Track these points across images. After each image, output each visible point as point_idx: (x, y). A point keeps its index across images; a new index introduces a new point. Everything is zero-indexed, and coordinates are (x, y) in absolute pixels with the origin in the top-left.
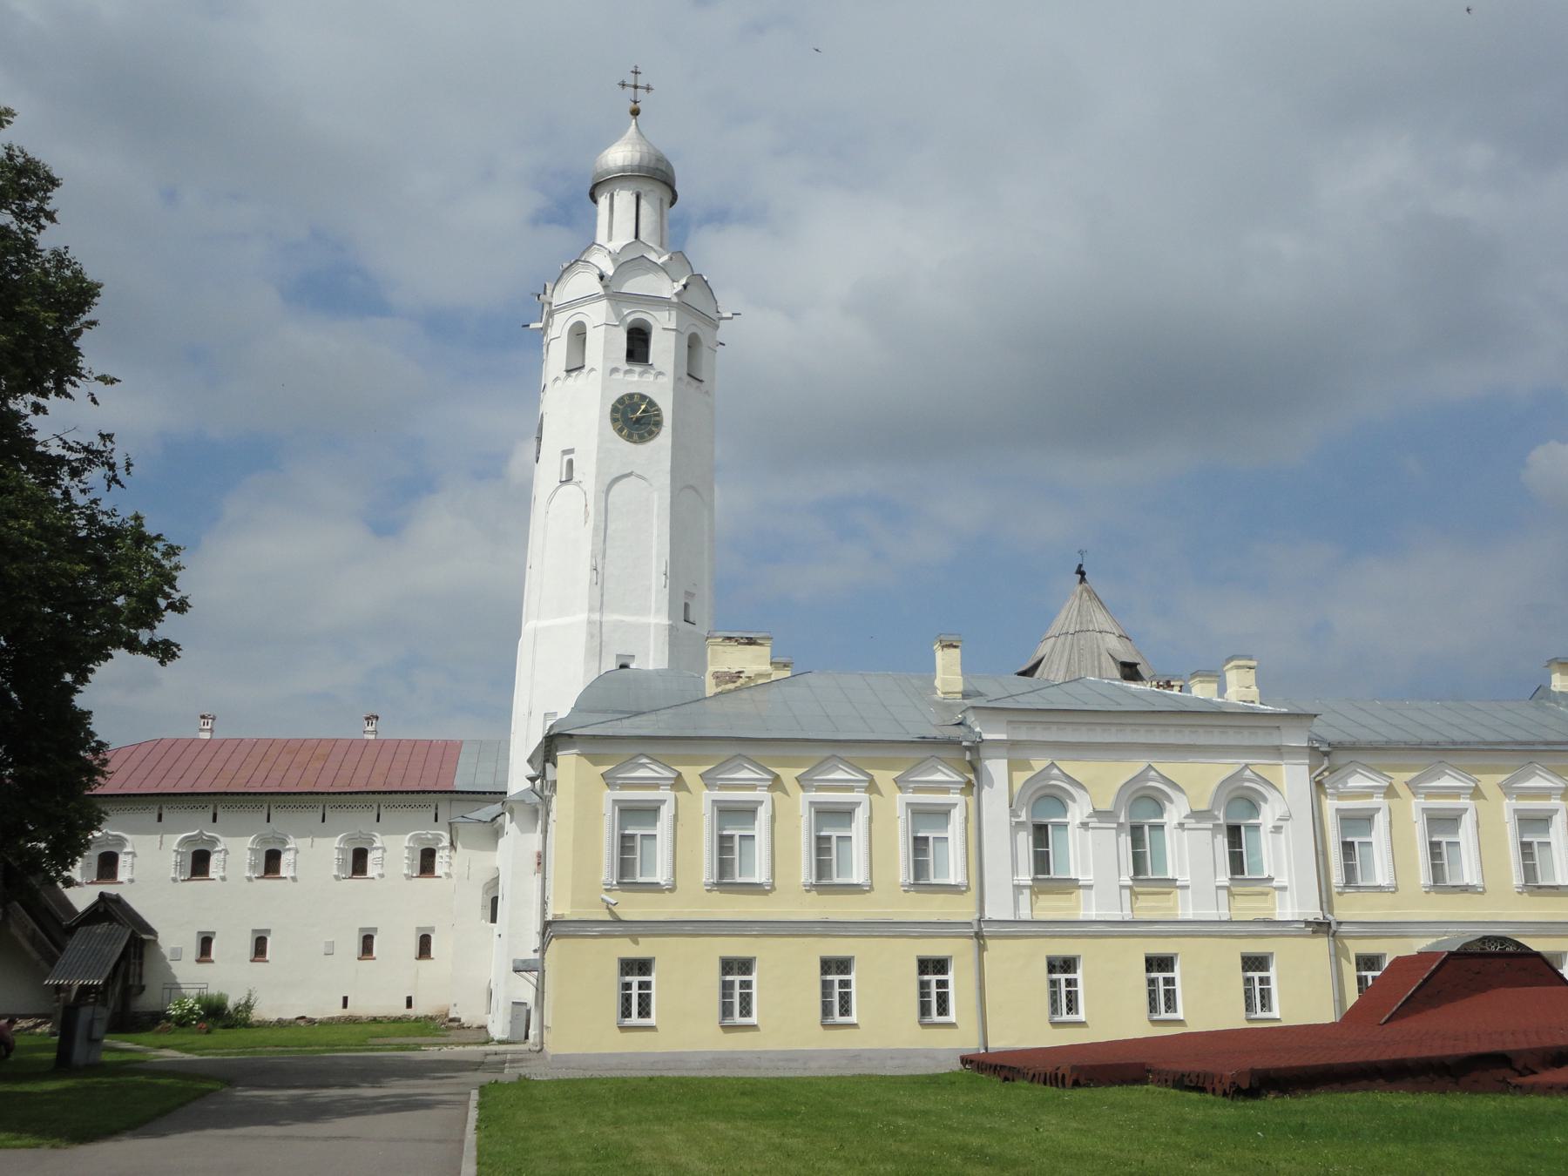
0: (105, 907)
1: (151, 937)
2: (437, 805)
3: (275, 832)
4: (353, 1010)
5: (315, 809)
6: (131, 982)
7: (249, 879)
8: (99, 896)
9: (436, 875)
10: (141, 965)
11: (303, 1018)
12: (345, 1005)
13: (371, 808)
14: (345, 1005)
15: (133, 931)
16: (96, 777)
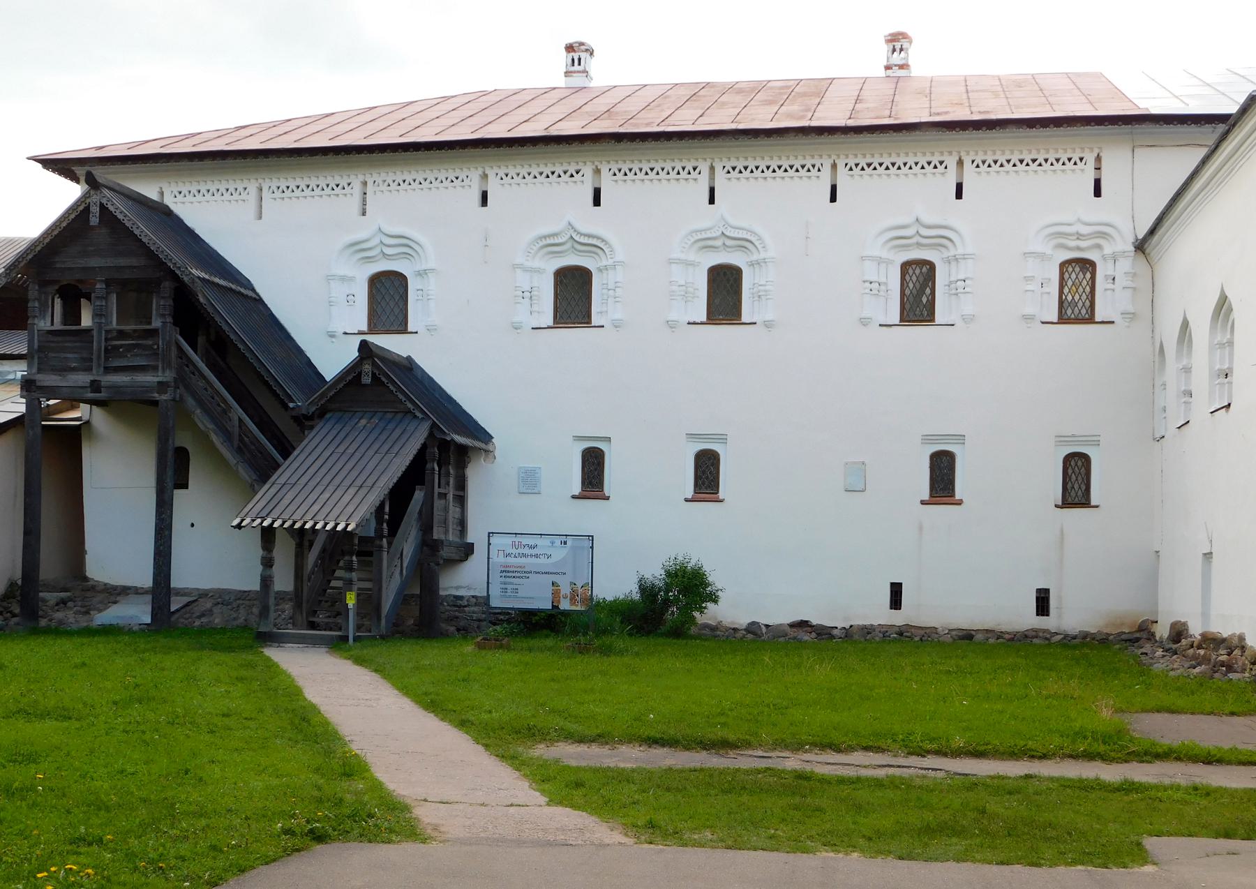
0: (374, 374)
1: (482, 445)
2: (1098, 159)
3: (727, 224)
4: (913, 613)
5: (814, 172)
6: (437, 534)
7: (864, 322)
8: (360, 350)
9: (745, 318)
10: (461, 500)
11: (803, 624)
12: (896, 602)
13: (941, 168)
14: (896, 602)
15: (434, 425)
16: (41, 594)
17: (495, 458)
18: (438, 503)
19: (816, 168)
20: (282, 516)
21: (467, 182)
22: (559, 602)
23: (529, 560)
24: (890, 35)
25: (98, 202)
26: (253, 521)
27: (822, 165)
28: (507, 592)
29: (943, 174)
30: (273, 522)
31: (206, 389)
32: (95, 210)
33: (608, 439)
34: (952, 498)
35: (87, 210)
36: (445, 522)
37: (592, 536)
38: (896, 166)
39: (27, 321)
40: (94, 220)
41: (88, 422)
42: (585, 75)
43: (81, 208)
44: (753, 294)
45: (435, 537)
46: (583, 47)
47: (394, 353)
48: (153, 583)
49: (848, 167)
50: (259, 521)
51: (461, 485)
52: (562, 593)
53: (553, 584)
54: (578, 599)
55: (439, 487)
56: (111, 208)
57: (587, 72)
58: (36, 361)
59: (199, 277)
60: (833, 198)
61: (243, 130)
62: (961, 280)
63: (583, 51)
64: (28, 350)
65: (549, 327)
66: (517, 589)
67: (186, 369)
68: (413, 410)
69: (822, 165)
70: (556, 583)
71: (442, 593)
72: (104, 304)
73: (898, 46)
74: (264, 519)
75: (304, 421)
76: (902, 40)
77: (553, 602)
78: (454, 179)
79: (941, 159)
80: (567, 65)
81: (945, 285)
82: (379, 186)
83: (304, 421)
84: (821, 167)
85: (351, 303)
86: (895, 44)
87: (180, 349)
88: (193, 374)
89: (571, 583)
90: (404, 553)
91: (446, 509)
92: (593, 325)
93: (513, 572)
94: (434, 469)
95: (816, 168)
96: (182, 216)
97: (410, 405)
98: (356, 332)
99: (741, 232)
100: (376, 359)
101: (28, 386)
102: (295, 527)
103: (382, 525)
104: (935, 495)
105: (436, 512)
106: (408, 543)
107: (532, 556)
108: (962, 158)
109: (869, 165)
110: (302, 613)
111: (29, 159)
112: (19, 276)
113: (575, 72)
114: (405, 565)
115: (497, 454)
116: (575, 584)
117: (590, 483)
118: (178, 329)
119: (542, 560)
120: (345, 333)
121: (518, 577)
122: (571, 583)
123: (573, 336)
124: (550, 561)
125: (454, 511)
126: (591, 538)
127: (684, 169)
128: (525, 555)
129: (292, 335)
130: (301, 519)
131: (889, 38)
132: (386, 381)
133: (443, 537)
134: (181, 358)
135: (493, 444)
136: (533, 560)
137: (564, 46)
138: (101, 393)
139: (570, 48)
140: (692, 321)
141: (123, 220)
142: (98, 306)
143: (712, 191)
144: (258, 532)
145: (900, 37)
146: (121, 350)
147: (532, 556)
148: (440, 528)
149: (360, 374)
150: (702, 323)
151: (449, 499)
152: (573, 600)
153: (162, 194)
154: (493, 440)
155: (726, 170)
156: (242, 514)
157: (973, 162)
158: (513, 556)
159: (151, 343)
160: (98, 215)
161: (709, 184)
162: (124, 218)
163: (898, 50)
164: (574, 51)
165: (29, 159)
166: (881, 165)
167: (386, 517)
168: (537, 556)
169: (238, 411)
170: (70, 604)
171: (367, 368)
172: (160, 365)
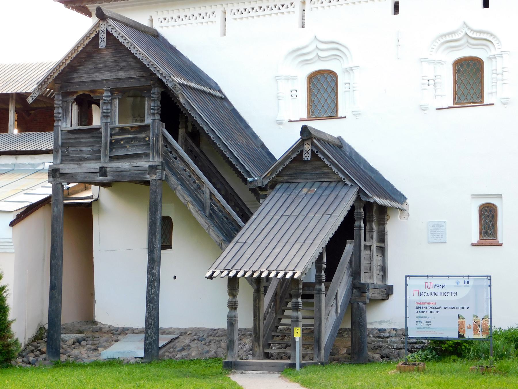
0: (312, 152)
8: (302, 133)
10: (382, 250)
17: (409, 215)
18: (364, 254)
20: (244, 268)
22: (464, 331)
23: (439, 297)
26: (222, 272)
31: (185, 170)
32: (103, 36)
33: (500, 196)
35: (97, 36)
37: (490, 277)
40: (102, 44)
41: (97, 200)
43: (93, 35)
45: (363, 281)
47: (328, 134)
52: (467, 325)
53: (459, 317)
54: (480, 329)
55: (365, 240)
56: (115, 34)
59: (179, 84)
66: (429, 322)
68: (344, 179)
70: (462, 316)
77: (459, 332)
83: (259, 191)
85: (294, 97)
87: (165, 139)
88: (176, 158)
89: (474, 316)
91: (371, 258)
94: (360, 226)
98: (299, 120)
100: (314, 140)
101: (54, 173)
107: (441, 294)
110: (259, 345)
112: (48, 89)
114: (339, 304)
116: (477, 317)
117: (486, 233)
118: (164, 124)
120: (290, 121)
122: (474, 316)
125: (377, 260)
128: (436, 294)
132: (322, 157)
133: (368, 281)
134: (166, 146)
136: (443, 297)
142: (105, 109)
146: (122, 142)
147: (441, 294)
149: (302, 152)
151: (373, 251)
153: (152, 21)
154: (407, 201)
156: (213, 268)
158: (426, 294)
159: (144, 136)
167: (324, 266)
169: (209, 186)
170: (83, 343)
172: (151, 153)
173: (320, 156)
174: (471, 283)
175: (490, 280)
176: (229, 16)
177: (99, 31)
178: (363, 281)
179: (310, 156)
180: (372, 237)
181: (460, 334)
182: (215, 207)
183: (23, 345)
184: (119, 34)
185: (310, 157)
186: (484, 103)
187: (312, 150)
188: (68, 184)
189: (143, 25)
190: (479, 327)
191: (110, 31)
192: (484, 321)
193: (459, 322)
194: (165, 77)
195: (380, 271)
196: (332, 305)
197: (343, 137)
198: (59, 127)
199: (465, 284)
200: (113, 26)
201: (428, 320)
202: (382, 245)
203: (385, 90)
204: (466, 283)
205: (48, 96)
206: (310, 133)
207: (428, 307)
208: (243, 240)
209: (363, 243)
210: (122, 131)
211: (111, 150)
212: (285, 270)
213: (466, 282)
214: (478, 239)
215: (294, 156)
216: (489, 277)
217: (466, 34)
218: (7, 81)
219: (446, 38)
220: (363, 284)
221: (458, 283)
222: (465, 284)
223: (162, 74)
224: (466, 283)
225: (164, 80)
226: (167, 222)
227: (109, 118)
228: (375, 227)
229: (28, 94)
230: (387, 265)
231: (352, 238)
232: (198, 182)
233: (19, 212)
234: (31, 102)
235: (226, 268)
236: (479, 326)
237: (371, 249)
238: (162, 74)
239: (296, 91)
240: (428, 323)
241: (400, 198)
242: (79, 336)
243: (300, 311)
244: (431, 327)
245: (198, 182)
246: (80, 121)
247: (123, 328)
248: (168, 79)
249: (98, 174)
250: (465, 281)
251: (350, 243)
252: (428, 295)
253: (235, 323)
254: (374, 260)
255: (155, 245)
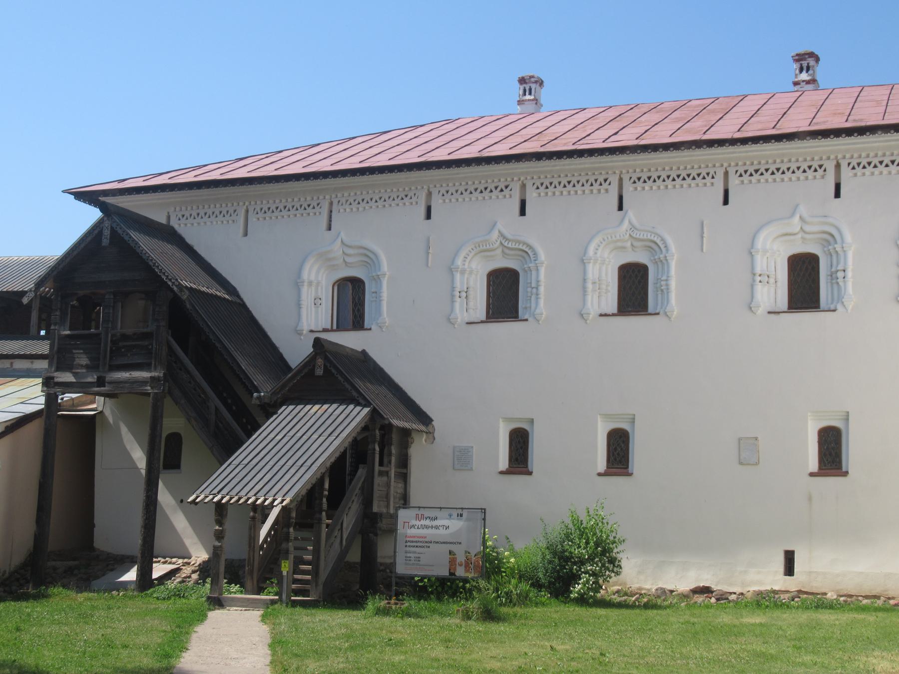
0: (325, 366)
5: (709, 180)
8: (314, 346)
10: (404, 477)
17: (434, 439)
18: (378, 481)
19: (710, 176)
20: (230, 494)
21: (414, 200)
22: (455, 569)
23: (430, 531)
24: (797, 55)
25: (109, 226)
26: (207, 497)
27: (715, 173)
28: (411, 560)
29: (823, 177)
30: (222, 498)
31: (190, 382)
32: (107, 233)
34: (839, 471)
35: (100, 233)
36: (387, 497)
37: (485, 509)
38: (781, 171)
39: (50, 327)
40: (105, 242)
41: (101, 412)
42: (535, 102)
43: (96, 232)
44: (657, 288)
45: (375, 509)
46: (533, 80)
47: (348, 348)
48: (361, 559)
49: (738, 174)
50: (211, 497)
51: (404, 463)
52: (458, 561)
53: (450, 553)
54: (472, 566)
55: (381, 464)
56: (120, 231)
57: (537, 100)
58: (55, 361)
59: (186, 287)
60: (726, 202)
61: (242, 161)
62: (841, 270)
63: (533, 83)
64: (50, 350)
65: (482, 322)
66: (419, 558)
67: (174, 365)
68: (358, 397)
69: (715, 173)
70: (453, 552)
71: (379, 560)
72: (111, 311)
73: (805, 64)
74: (215, 495)
75: (268, 408)
76: (808, 59)
77: (450, 570)
78: (404, 197)
79: (821, 163)
80: (520, 95)
81: (828, 275)
82: (342, 205)
83: (268, 408)
84: (714, 175)
86: (803, 62)
87: (170, 348)
88: (181, 369)
89: (466, 552)
90: (345, 525)
91: (388, 485)
92: (520, 319)
93: (416, 542)
94: (374, 449)
95: (710, 176)
96: (184, 235)
97: (355, 394)
99: (641, 237)
100: (327, 354)
101: (48, 383)
102: (257, 503)
103: (322, 500)
104: (824, 468)
105: (376, 487)
106: (349, 518)
107: (432, 527)
108: (839, 162)
109: (893, 162)
110: (252, 578)
111: (64, 191)
112: (47, 289)
113: (526, 100)
114: (345, 536)
115: (436, 435)
116: (469, 553)
117: (517, 460)
118: (170, 331)
119: (442, 531)
121: (420, 547)
122: (466, 552)
123: (504, 329)
124: (448, 532)
125: (396, 487)
126: (483, 511)
127: (596, 181)
128: (427, 527)
129: (269, 334)
130: (246, 495)
131: (797, 58)
132: (336, 373)
133: (384, 510)
134: (171, 356)
135: (433, 426)
136: (434, 531)
137: (518, 79)
138: (105, 387)
139: (522, 81)
140: (603, 313)
141: (129, 241)
142: (106, 313)
143: (621, 198)
144: (214, 506)
145: (807, 57)
146: (123, 350)
147: (432, 527)
148: (381, 502)
149: (314, 366)
150: (613, 315)
151: (390, 477)
152: (467, 565)
153: (169, 217)
154: (433, 423)
155: (632, 181)
156: (198, 492)
157: (849, 164)
158: (416, 527)
159: (146, 343)
160: (108, 237)
161: (835, 181)
162: (129, 239)
163: (805, 68)
164: (526, 83)
165: (64, 191)
166: (767, 170)
167: (326, 493)
168: (437, 527)
169: (215, 401)
170: (76, 572)
171: (320, 361)
172: (153, 363)
173: (334, 371)
174: (465, 515)
175: (485, 513)
176: (252, 218)
177: (103, 227)
178: (375, 509)
179: (322, 371)
180: (390, 462)
181: (451, 571)
182: (220, 424)
183: (7, 572)
184: (124, 232)
185: (322, 373)
186: (518, 318)
187: (325, 365)
188: (63, 394)
189: (156, 221)
190: (471, 565)
191: (115, 228)
192: (476, 558)
193: (450, 558)
194: (170, 280)
195: (399, 500)
196: (336, 537)
197: (367, 351)
198: (56, 331)
199: (458, 516)
200: (117, 223)
201: (417, 555)
202: (405, 471)
203: (414, 301)
204: (459, 516)
205: (48, 296)
206: (323, 346)
207: (418, 542)
208: (236, 462)
209: (377, 467)
210: (125, 337)
211: (111, 359)
212: (264, 496)
213: (459, 514)
214: (606, 468)
215: (306, 370)
216: (484, 511)
217: (501, 243)
218: (5, 278)
219: (522, 246)
220: (376, 514)
221: (450, 516)
222: (458, 516)
223: (167, 276)
224: (459, 516)
225: (170, 283)
226: (175, 440)
227: (582, 313)
228: (393, 451)
229: (23, 293)
230: (409, 492)
231: (364, 462)
232: (203, 396)
233: (8, 424)
234: (26, 303)
235: (212, 493)
236: (471, 563)
237: (389, 475)
238: (167, 276)
239: (320, 299)
240: (417, 559)
241: (425, 419)
242: (72, 563)
243: (291, 542)
244: (421, 563)
245: (203, 396)
246: (624, 314)
247: (123, 556)
248: (174, 282)
249: (96, 384)
250: (458, 514)
251: (363, 468)
252: (418, 528)
253: (221, 555)
254: (392, 488)
255: (153, 464)
